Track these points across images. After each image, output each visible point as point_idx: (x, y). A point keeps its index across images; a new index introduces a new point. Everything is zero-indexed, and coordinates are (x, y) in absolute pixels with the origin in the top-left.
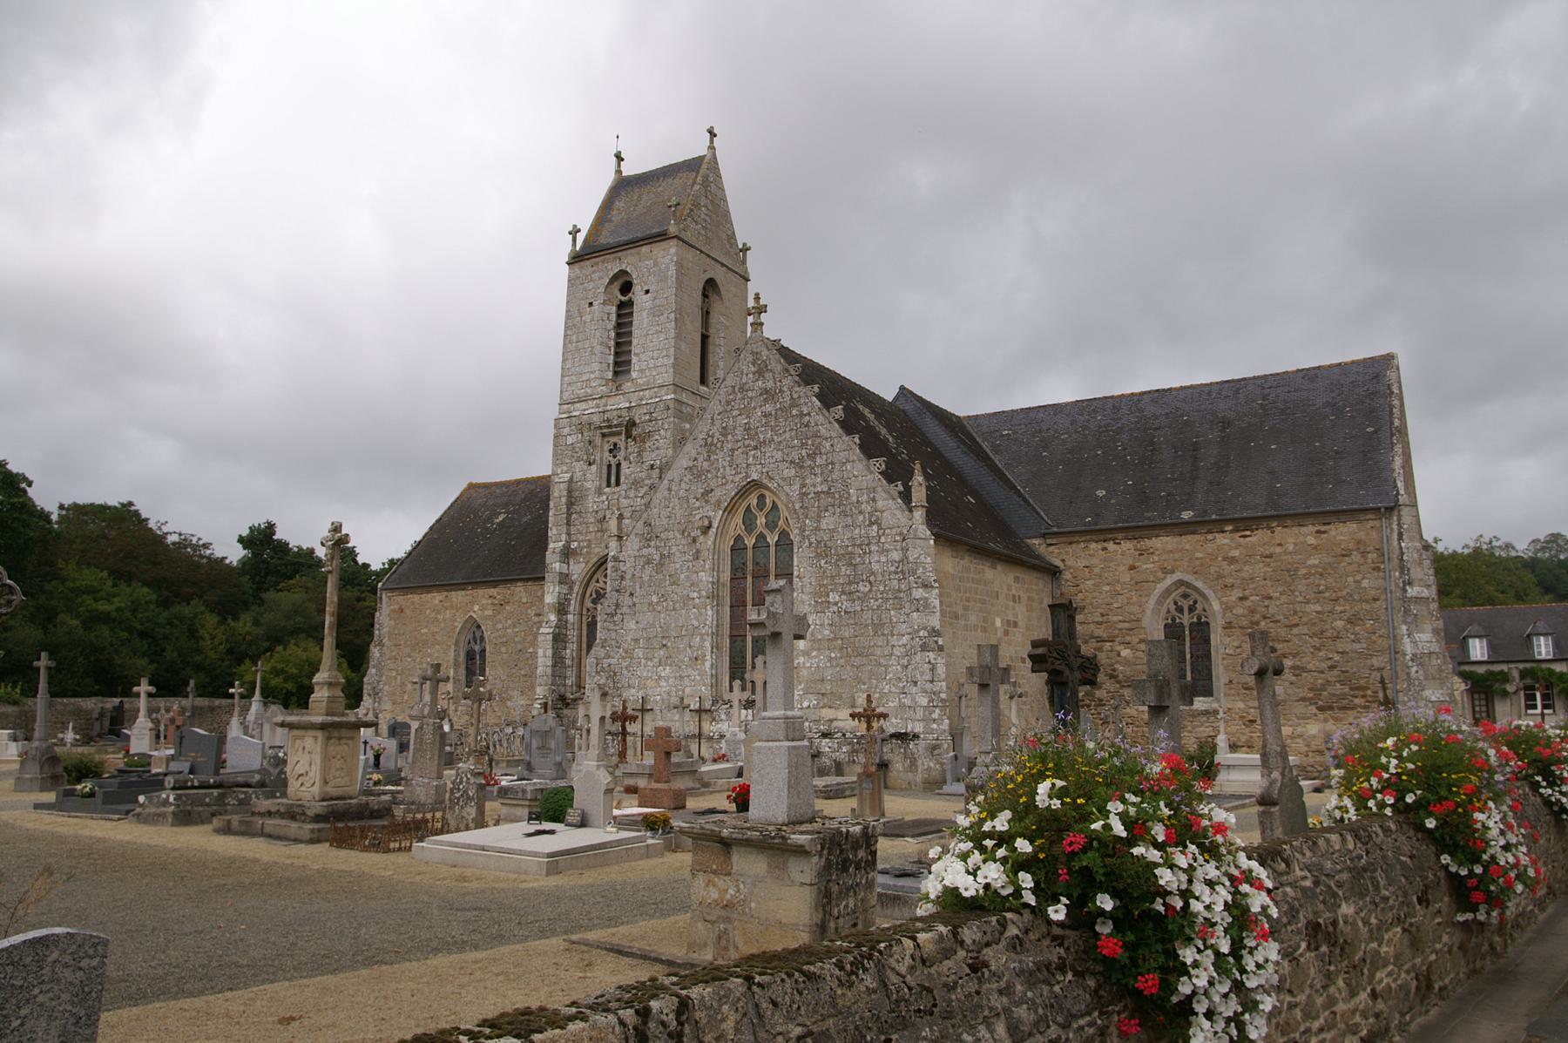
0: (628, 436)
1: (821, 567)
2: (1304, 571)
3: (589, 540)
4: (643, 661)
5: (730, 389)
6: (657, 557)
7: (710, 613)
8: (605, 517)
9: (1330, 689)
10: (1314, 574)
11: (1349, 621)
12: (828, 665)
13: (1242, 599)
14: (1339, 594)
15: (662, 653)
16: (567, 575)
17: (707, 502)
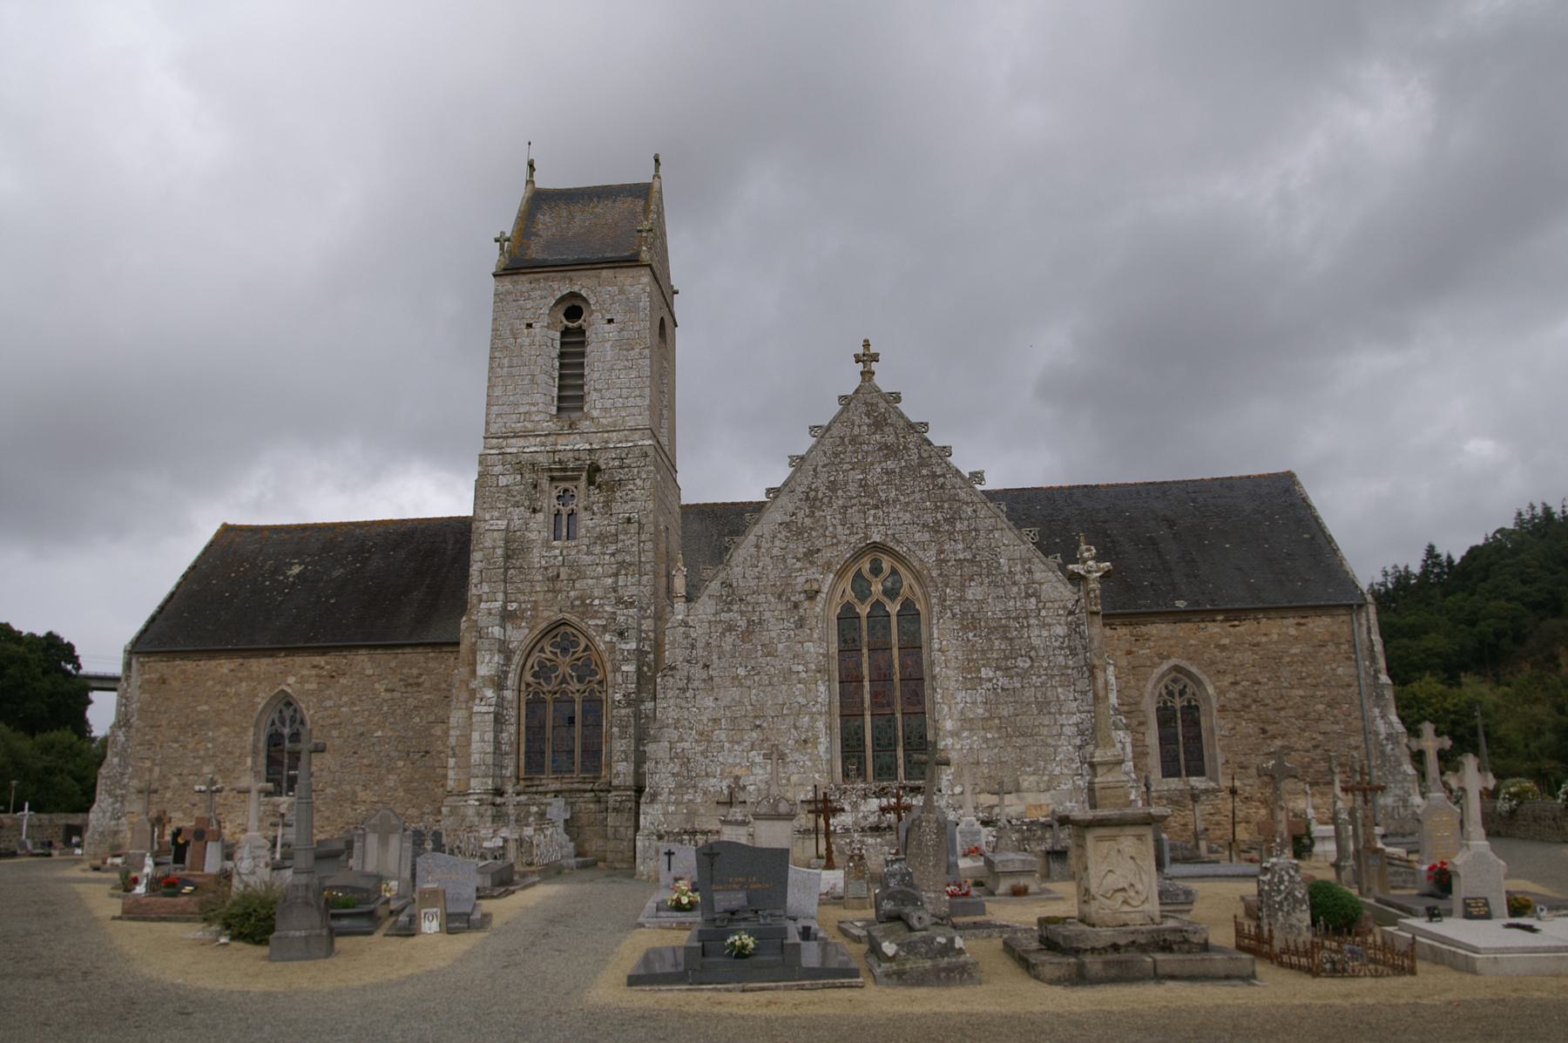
0: (591, 482)
1: (969, 640)
2: (1288, 659)
3: (535, 602)
4: (727, 745)
5: (838, 441)
6: (743, 623)
7: (822, 688)
8: (558, 576)
9: (1316, 766)
10: (1296, 662)
11: (1329, 705)
12: (984, 746)
13: (1235, 683)
14: (1319, 680)
15: (754, 735)
16: (504, 642)
17: (812, 563)
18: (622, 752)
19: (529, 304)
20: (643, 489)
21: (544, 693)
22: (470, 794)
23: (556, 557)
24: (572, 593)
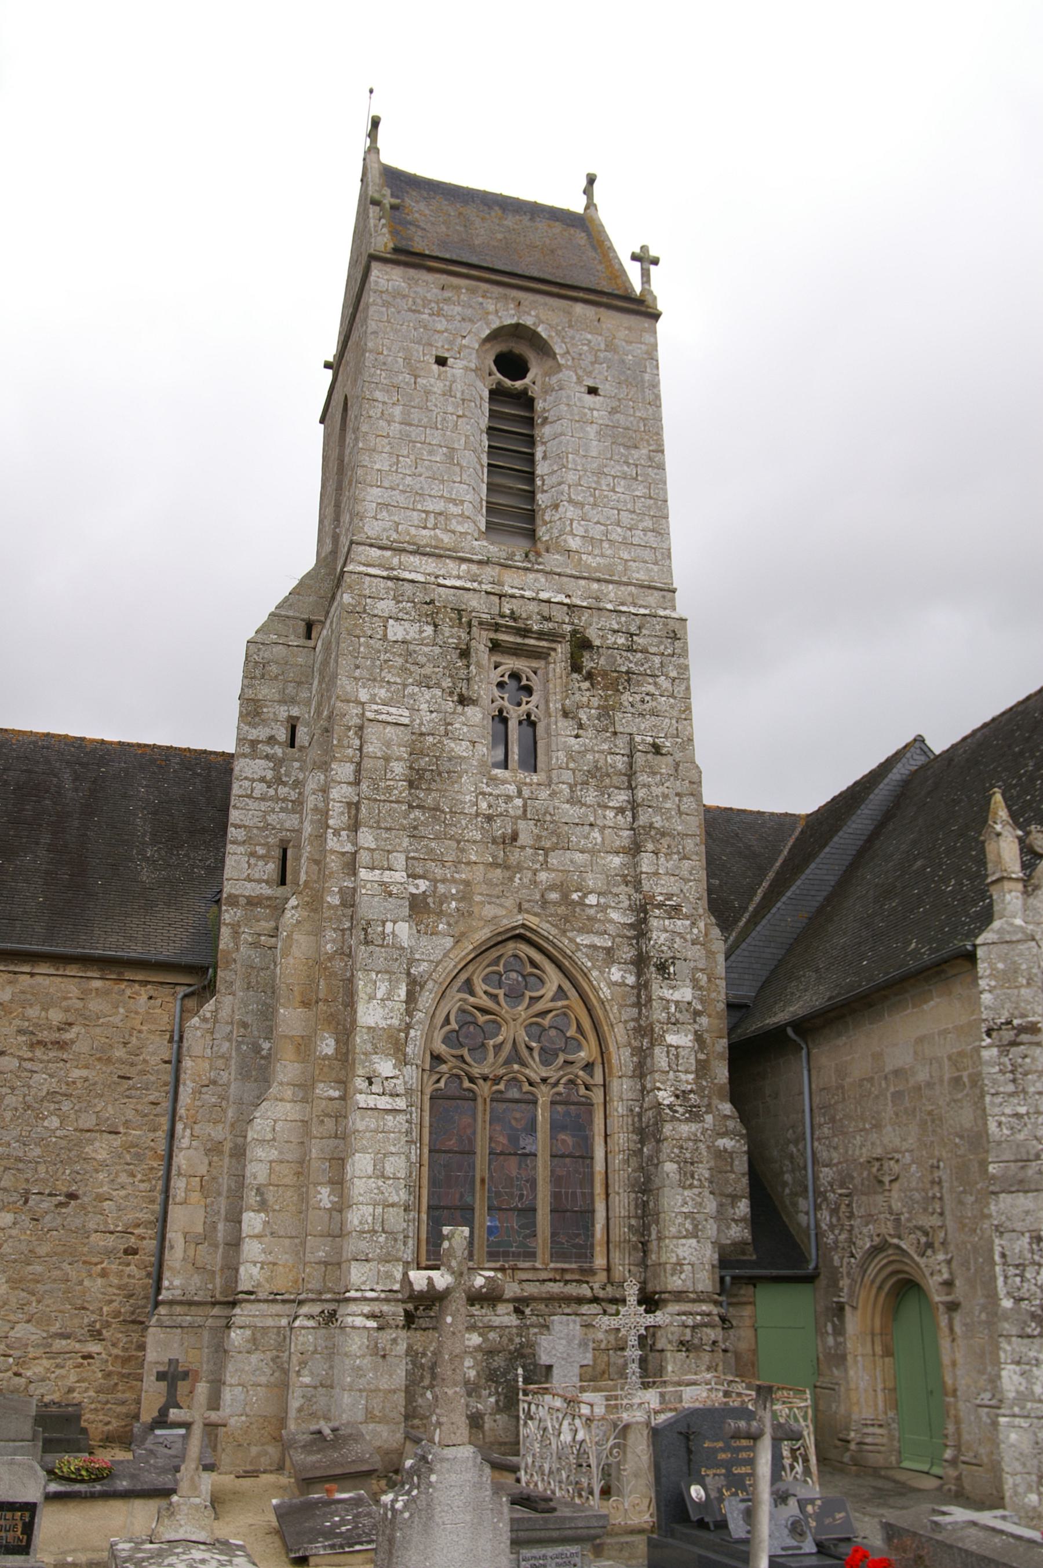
3: (467, 883)
8: (515, 837)
18: (687, 1216)
19: (441, 324)
20: (672, 696)
21: (472, 1080)
22: (348, 1300)
23: (509, 798)
24: (543, 876)
